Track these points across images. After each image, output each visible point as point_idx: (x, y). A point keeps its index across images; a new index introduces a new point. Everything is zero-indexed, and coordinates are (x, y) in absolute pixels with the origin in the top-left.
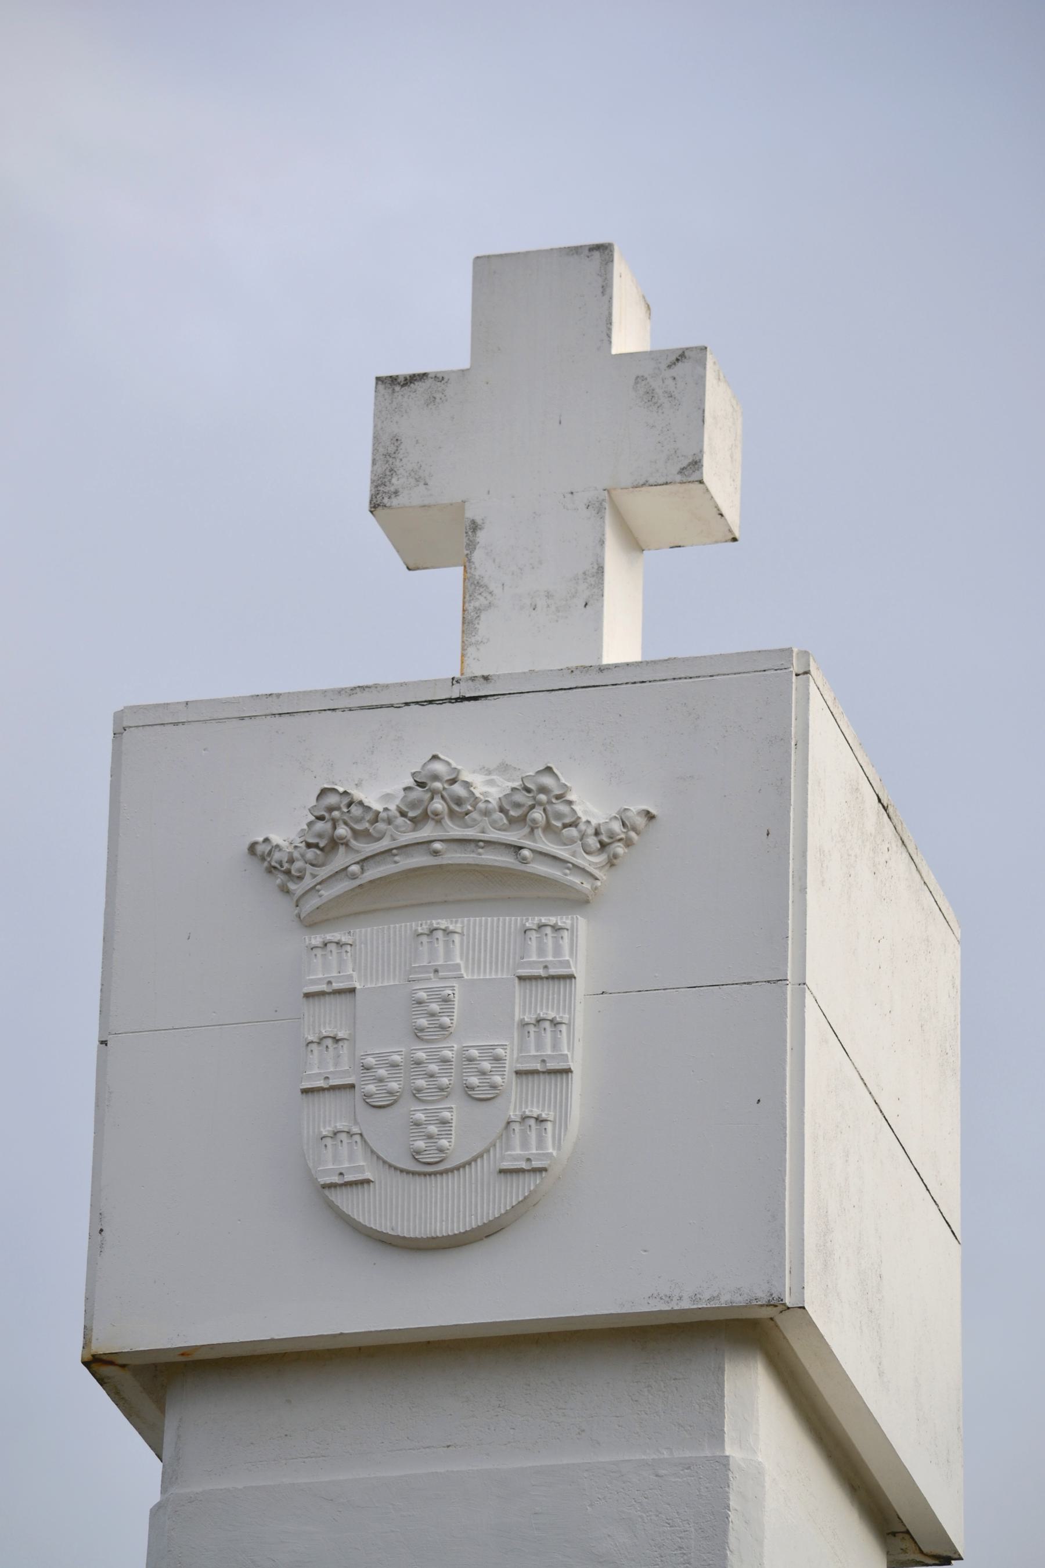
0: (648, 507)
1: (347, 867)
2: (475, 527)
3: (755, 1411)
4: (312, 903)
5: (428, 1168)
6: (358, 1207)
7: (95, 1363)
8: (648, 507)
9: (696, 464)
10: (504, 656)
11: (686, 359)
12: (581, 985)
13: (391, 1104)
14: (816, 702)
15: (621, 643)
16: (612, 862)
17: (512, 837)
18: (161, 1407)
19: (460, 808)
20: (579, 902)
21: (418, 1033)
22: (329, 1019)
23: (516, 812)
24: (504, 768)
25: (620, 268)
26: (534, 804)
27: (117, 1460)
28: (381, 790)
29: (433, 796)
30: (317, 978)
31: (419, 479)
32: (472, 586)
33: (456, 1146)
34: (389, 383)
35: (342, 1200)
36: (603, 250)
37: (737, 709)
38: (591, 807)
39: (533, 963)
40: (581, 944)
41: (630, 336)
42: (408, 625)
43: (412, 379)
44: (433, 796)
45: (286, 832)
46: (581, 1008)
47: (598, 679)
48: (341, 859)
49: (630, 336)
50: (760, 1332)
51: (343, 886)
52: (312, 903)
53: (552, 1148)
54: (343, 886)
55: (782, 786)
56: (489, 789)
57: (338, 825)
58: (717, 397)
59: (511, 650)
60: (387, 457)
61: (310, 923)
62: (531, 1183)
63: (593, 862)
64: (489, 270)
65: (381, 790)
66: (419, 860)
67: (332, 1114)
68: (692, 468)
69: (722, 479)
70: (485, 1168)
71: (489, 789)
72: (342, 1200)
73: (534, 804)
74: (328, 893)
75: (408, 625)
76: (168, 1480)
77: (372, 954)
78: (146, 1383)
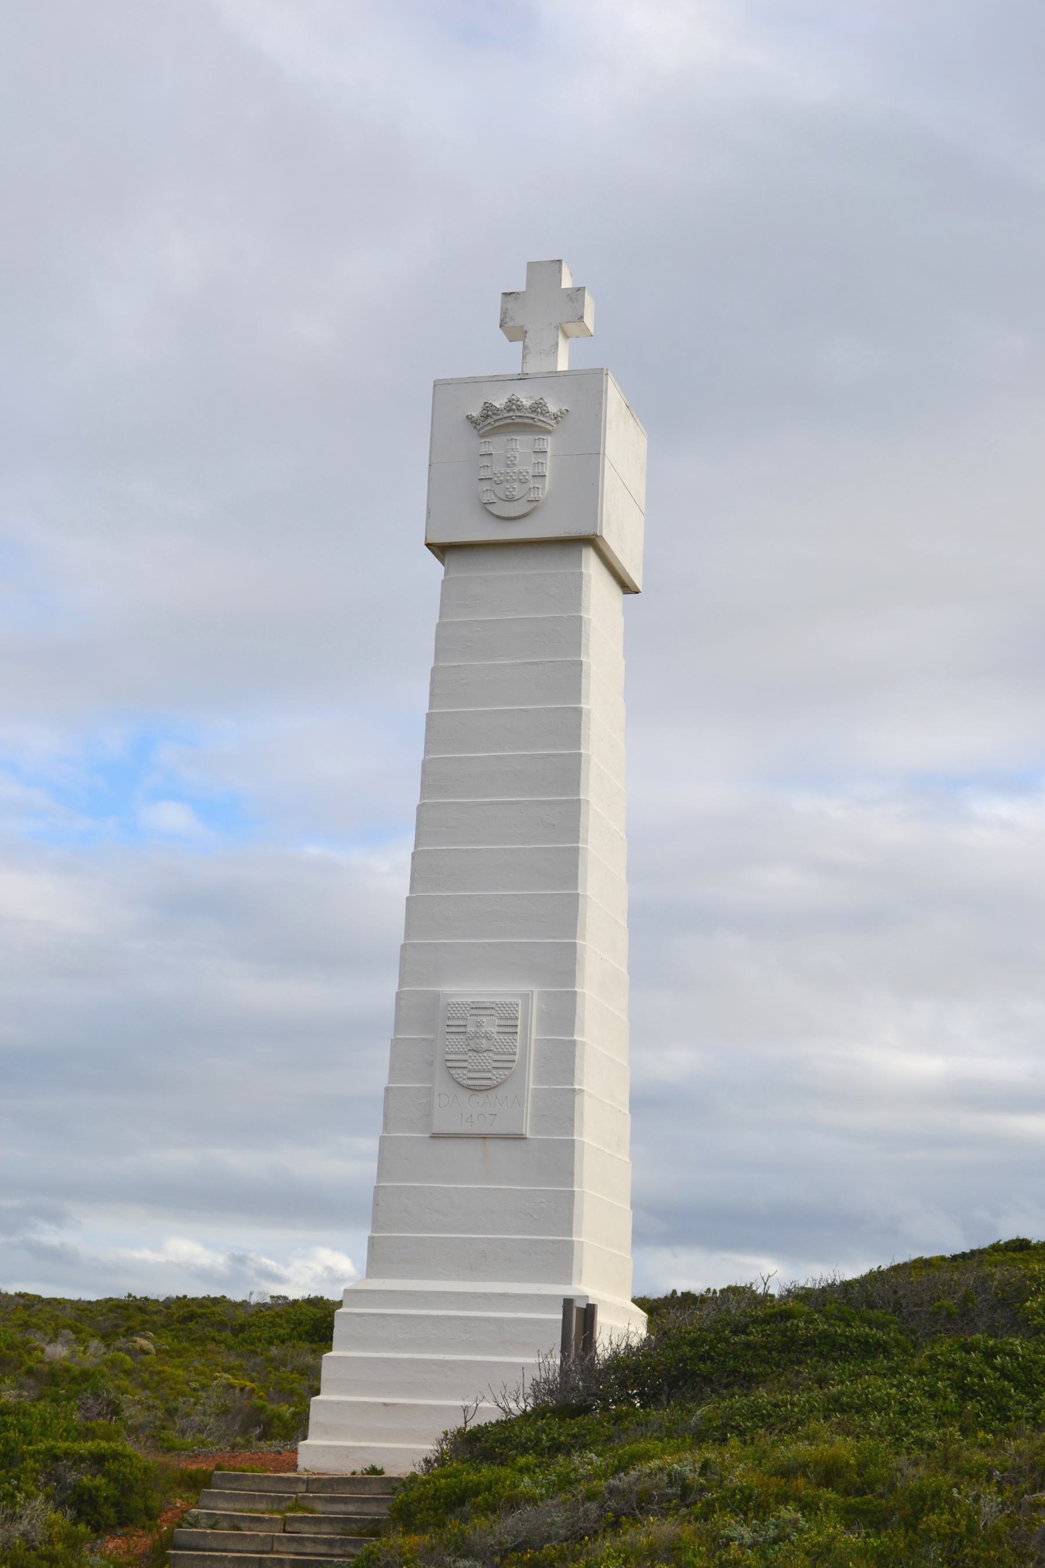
0: (570, 328)
1: (497, 422)
2: (526, 332)
3: (591, 564)
4: (482, 431)
5: (510, 500)
6: (492, 509)
7: (428, 545)
8: (570, 328)
9: (582, 317)
10: (531, 369)
11: (580, 290)
12: (549, 454)
13: (491, 1088)
14: (610, 381)
15: (563, 365)
16: (557, 422)
17: (532, 415)
18: (444, 555)
19: (519, 408)
20: (549, 432)
21: (508, 466)
22: (486, 461)
23: (534, 409)
24: (531, 397)
25: (564, 266)
26: (538, 407)
27: (434, 568)
28: (499, 403)
29: (513, 405)
30: (483, 451)
31: (512, 319)
32: (525, 347)
33: (517, 494)
34: (505, 294)
35: (489, 507)
36: (560, 261)
37: (588, 384)
38: (553, 408)
39: (537, 448)
40: (549, 444)
41: (567, 283)
42: (505, 357)
43: (511, 293)
44: (513, 405)
45: (475, 413)
46: (549, 459)
47: (556, 374)
48: (489, 420)
49: (567, 283)
50: (592, 541)
51: (490, 427)
52: (482, 431)
53: (540, 495)
54: (490, 427)
55: (601, 404)
56: (527, 403)
57: (489, 411)
58: (588, 300)
59: (534, 367)
60: (504, 313)
61: (482, 436)
62: (535, 504)
63: (552, 422)
64: (531, 265)
65: (499, 403)
66: (509, 421)
67: (486, 485)
68: (581, 318)
69: (589, 321)
70: (524, 500)
71: (527, 403)
72: (489, 507)
73: (538, 407)
74: (486, 429)
75: (505, 357)
76: (446, 573)
77: (496, 445)
78: (441, 550)
